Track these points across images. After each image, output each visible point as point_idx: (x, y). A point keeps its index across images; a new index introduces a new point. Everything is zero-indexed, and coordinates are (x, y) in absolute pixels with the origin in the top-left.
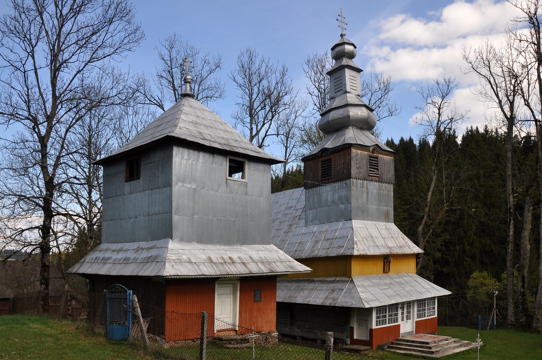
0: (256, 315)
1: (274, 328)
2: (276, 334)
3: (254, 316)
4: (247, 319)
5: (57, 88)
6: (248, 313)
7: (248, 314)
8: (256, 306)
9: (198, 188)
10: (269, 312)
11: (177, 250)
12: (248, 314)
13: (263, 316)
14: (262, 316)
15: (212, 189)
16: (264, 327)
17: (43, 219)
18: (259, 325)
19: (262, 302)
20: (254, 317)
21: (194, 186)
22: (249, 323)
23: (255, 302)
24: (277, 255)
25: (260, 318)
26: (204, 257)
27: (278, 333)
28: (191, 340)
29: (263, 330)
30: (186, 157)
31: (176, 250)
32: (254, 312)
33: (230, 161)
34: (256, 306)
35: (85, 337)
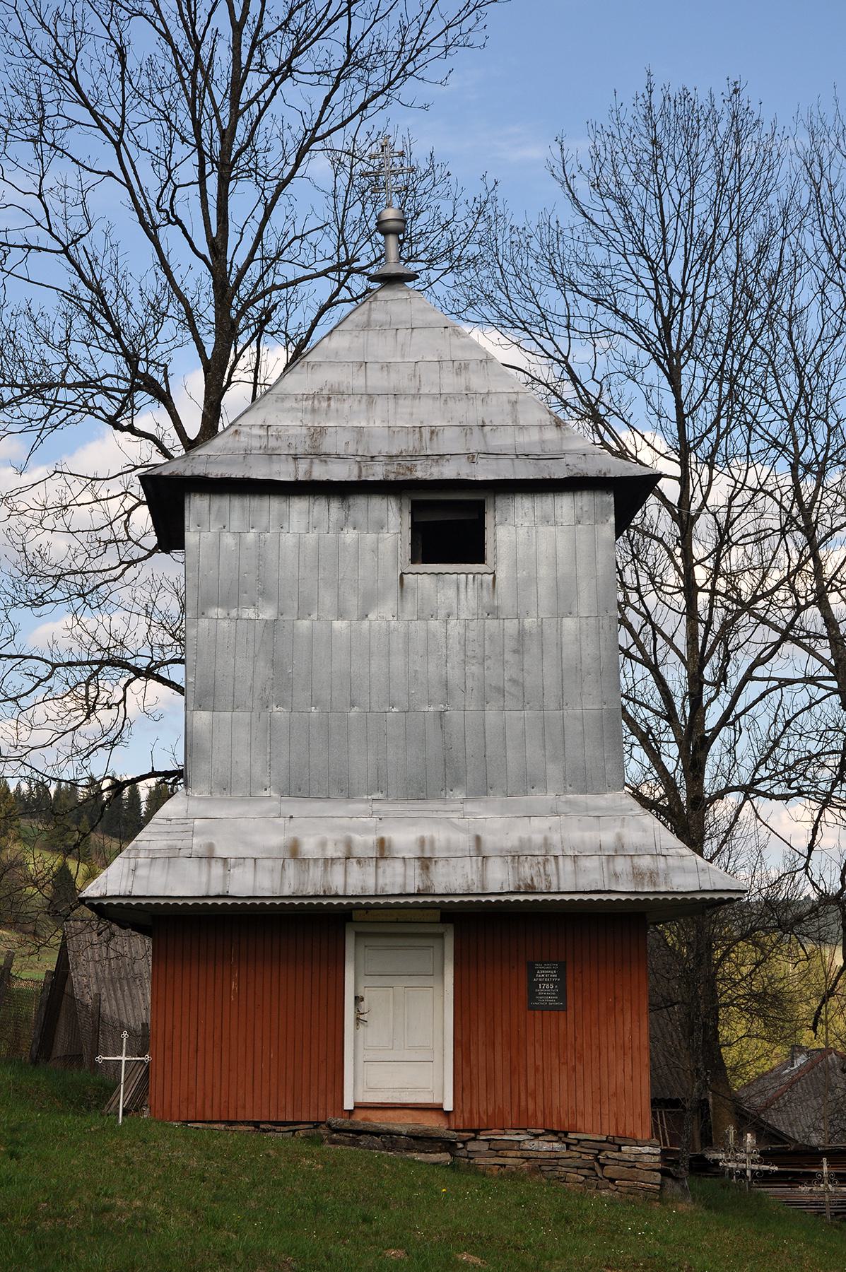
0: (539, 1063)
1: (638, 1118)
2: (648, 1152)
3: (530, 1062)
4: (499, 1074)
5: (648, 796)
6: (498, 1048)
7: (498, 1057)
8: (538, 1027)
9: (285, 617)
10: (612, 1055)
11: (184, 821)
12: (498, 1057)
13: (579, 1068)
14: (574, 1069)
15: (341, 615)
16: (583, 1115)
17: (119, 779)
18: (556, 1102)
19: (570, 1013)
20: (531, 1071)
21: (268, 613)
22: (508, 1090)
23: (532, 1008)
24: (617, 830)
25: (564, 1077)
26: (276, 840)
27: (658, 1151)
28: (248, 1123)
29: (580, 1124)
30: (236, 523)
31: (179, 822)
32: (530, 1049)
33: (416, 508)
34: (538, 1027)
35: (722, 799)
